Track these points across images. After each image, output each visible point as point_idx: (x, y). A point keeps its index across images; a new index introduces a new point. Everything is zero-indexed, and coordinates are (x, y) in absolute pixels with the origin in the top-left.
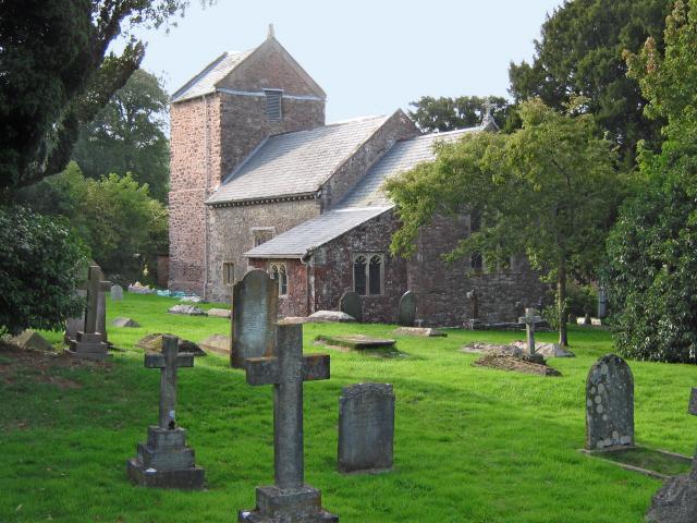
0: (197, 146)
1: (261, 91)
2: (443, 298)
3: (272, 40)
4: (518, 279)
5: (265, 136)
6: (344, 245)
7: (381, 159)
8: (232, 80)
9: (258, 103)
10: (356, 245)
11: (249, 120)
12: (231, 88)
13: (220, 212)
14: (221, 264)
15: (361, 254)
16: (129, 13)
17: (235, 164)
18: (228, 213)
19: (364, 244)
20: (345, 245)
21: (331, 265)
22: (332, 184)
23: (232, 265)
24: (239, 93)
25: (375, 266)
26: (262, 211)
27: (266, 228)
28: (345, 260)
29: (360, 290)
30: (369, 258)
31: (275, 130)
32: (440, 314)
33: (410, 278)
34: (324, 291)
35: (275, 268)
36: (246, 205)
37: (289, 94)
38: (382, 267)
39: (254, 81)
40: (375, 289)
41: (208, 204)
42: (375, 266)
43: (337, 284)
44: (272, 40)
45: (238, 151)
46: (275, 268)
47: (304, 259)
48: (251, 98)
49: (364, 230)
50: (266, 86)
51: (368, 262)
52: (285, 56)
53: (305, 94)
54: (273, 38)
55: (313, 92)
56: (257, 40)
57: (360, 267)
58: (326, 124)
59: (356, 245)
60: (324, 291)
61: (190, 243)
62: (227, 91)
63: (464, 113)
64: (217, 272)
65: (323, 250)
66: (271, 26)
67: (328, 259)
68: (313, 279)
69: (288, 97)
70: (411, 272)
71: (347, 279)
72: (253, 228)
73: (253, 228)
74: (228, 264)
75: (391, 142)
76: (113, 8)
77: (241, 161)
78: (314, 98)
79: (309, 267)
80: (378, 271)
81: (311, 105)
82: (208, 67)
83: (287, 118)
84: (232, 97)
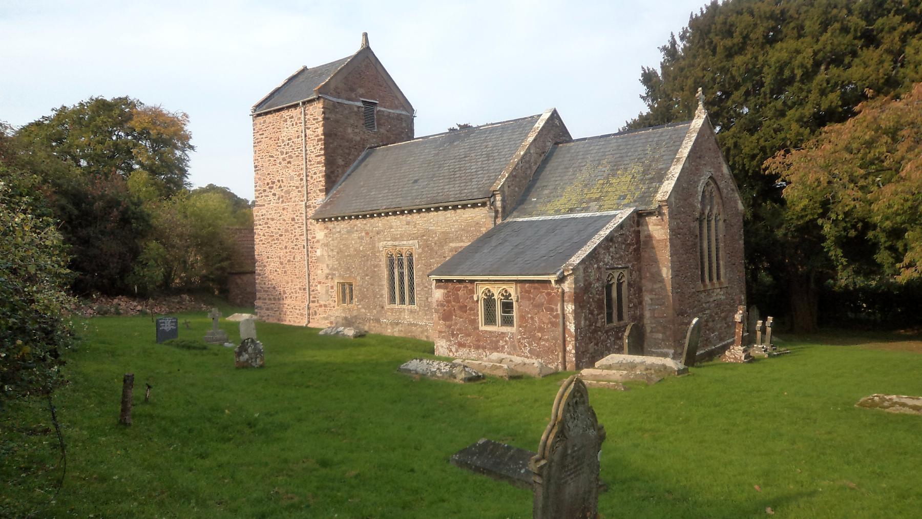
0: (290, 157)
6: (598, 262)
8: (332, 86)
9: (357, 113)
11: (350, 130)
12: (331, 95)
18: (343, 226)
22: (506, 189)
24: (340, 101)
26: (396, 222)
29: (610, 320)
37: (381, 106)
39: (352, 90)
48: (350, 107)
50: (362, 96)
51: (615, 281)
52: (378, 67)
53: (397, 108)
56: (352, 48)
61: (285, 261)
62: (328, 97)
66: (366, 35)
69: (382, 109)
75: (549, 145)
78: (404, 113)
79: (563, 292)
83: (382, 130)
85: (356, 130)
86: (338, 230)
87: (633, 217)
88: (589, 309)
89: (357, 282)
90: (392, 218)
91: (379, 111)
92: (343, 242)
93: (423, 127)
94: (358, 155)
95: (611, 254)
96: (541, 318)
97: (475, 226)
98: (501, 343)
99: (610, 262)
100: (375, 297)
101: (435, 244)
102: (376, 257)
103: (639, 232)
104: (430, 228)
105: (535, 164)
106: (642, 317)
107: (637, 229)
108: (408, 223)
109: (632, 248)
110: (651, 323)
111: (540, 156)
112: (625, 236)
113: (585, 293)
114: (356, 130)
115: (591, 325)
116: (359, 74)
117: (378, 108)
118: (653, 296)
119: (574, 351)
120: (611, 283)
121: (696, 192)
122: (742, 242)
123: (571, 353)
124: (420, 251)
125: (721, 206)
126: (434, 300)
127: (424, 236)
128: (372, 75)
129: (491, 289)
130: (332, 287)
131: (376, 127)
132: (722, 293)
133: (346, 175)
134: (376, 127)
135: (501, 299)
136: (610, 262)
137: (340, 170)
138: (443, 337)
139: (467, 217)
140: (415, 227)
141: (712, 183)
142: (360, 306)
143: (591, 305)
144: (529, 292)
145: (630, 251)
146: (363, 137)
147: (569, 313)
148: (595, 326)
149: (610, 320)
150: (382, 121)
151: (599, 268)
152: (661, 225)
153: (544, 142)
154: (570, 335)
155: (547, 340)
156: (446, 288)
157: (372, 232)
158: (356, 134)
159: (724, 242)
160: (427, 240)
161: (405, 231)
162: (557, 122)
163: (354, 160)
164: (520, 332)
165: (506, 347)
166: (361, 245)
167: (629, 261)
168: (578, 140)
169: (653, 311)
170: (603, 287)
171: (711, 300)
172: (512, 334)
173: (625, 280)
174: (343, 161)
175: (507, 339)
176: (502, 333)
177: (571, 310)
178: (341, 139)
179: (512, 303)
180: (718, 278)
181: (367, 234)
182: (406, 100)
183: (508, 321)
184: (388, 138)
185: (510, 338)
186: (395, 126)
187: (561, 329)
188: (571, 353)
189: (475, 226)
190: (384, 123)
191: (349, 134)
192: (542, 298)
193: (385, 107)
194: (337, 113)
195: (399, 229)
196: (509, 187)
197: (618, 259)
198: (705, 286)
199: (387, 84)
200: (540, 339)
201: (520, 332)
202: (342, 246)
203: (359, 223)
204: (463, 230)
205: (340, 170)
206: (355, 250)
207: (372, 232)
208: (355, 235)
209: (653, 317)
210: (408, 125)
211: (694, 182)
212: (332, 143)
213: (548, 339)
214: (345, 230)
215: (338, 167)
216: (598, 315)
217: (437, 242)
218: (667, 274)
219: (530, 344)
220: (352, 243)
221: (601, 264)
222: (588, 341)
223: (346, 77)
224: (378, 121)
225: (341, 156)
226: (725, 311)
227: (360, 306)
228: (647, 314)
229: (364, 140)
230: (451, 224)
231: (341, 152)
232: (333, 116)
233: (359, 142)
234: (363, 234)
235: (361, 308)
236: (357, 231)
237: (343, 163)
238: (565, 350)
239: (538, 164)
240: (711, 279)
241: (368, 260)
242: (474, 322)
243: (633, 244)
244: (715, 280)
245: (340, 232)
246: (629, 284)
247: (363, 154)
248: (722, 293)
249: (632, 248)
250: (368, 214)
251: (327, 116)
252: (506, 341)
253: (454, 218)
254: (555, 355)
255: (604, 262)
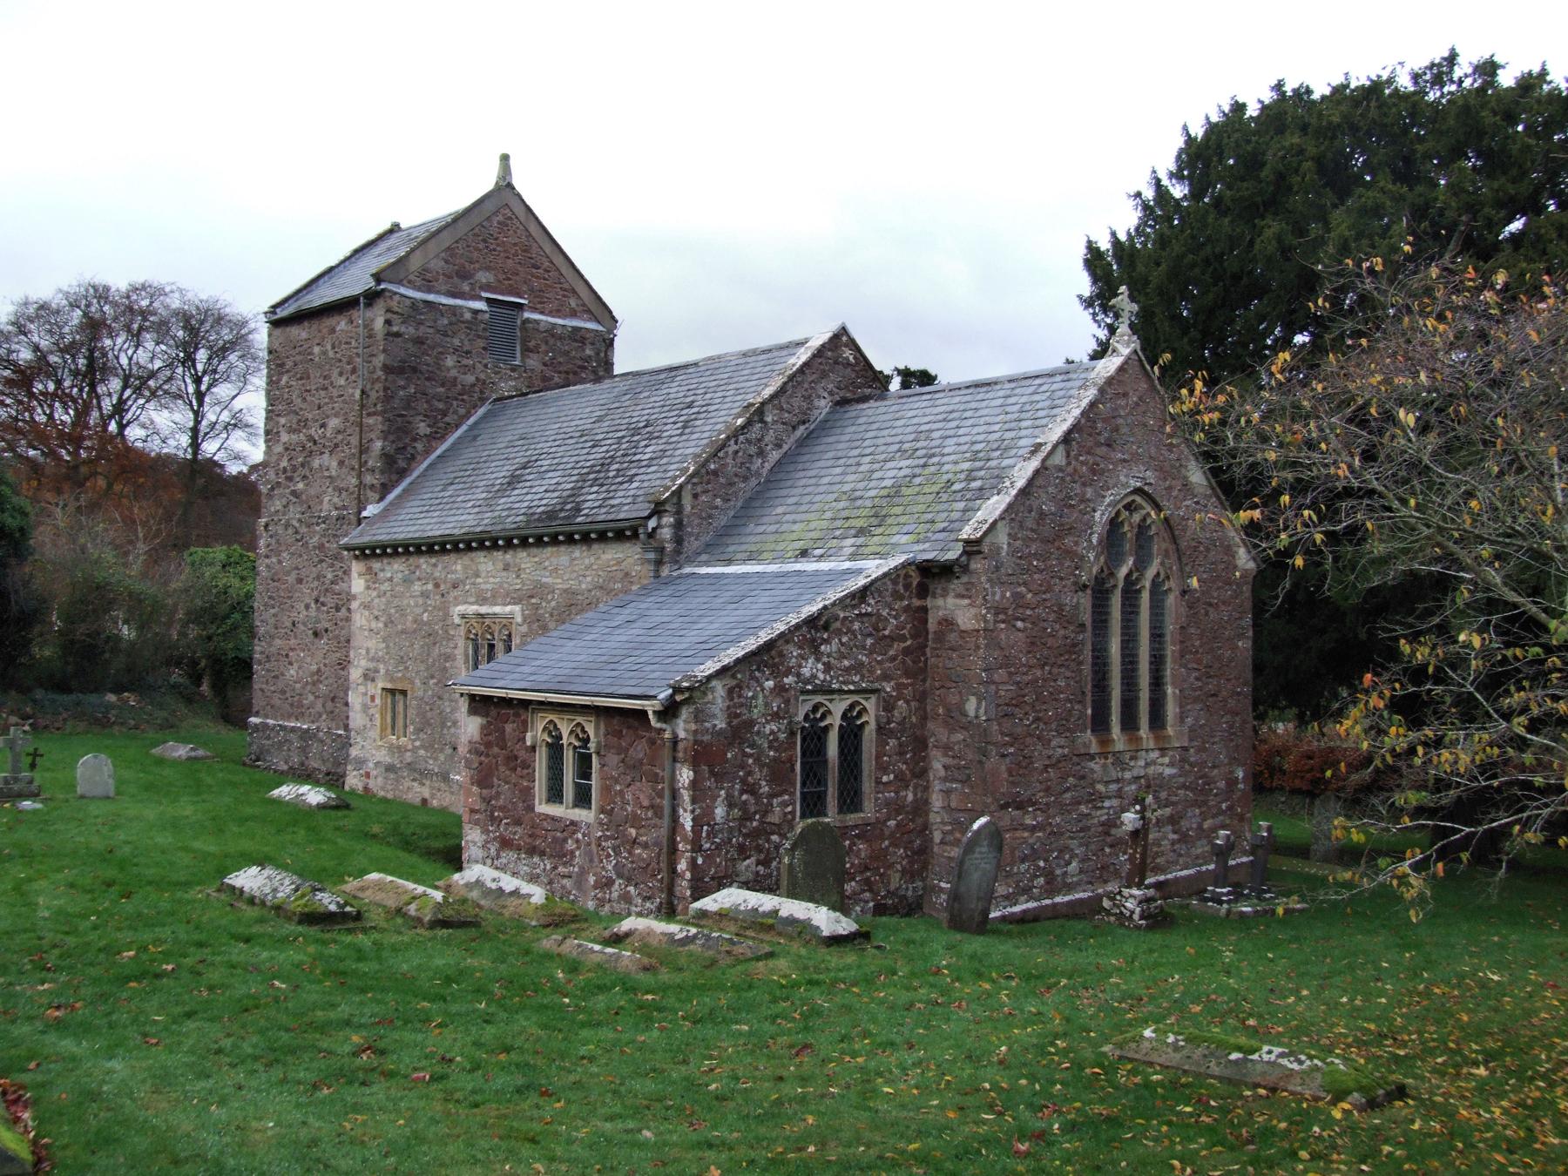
1: (480, 298)
2: (1029, 821)
3: (505, 186)
4: (1183, 760)
5: (483, 400)
7: (803, 443)
8: (416, 263)
9: (470, 325)
10: (806, 672)
11: (450, 361)
12: (411, 284)
13: (376, 565)
14: (376, 688)
15: (819, 699)
16: (229, 544)
17: (413, 457)
18: (395, 569)
19: (828, 668)
20: (777, 671)
21: (740, 730)
23: (404, 693)
24: (431, 297)
25: (851, 734)
26: (488, 566)
27: (497, 609)
28: (776, 716)
29: (814, 804)
30: (838, 707)
31: (506, 387)
32: (1023, 867)
33: (938, 764)
34: (720, 812)
35: (552, 729)
36: (444, 551)
37: (534, 310)
38: (870, 732)
39: (464, 275)
40: (851, 799)
41: (349, 548)
42: (851, 734)
43: (752, 790)
44: (505, 186)
45: (423, 428)
46: (552, 729)
47: (659, 714)
48: (453, 310)
49: (826, 627)
50: (488, 288)
51: (835, 720)
53: (573, 314)
54: (510, 186)
55: (589, 311)
56: (485, 183)
57: (814, 737)
58: (617, 370)
59: (806, 672)
60: (720, 812)
62: (402, 290)
63: (1094, 315)
64: (365, 708)
65: (719, 688)
66: (505, 158)
67: (731, 715)
68: (685, 775)
70: (947, 748)
71: (780, 775)
72: (461, 608)
73: (461, 608)
74: (392, 692)
76: (200, 367)
77: (428, 452)
79: (675, 741)
80: (857, 748)
81: (583, 341)
82: (356, 252)
84: (414, 304)
85: (465, 362)
86: (389, 575)
87: (907, 576)
88: (744, 781)
89: (418, 690)
90: (480, 557)
91: (528, 321)
92: (396, 602)
93: (625, 359)
94: (468, 416)
95: (825, 659)
96: (637, 795)
97: (622, 580)
98: (570, 845)
99: (821, 676)
100: (443, 725)
101: (552, 615)
102: (450, 638)
103: (925, 610)
104: (544, 580)
105: (779, 446)
106: (921, 807)
107: (916, 602)
108: (506, 568)
109: (897, 647)
110: (943, 823)
111: (794, 428)
112: (874, 619)
113: (731, 744)
114: (465, 362)
115: (746, 817)
116: (485, 241)
117: (527, 315)
118: (949, 761)
119: (688, 875)
120: (822, 724)
121: (1090, 525)
122: (1245, 645)
123: (683, 879)
124: (524, 629)
125: (1174, 557)
126: (464, 739)
127: (532, 597)
128: (515, 244)
129: (556, 721)
130: (373, 698)
131: (518, 355)
132: (1167, 760)
133: (433, 456)
134: (518, 355)
135: (575, 747)
136: (821, 676)
137: (419, 446)
138: (477, 823)
139: (609, 560)
140: (518, 576)
141: (1144, 504)
142: (418, 743)
143: (750, 773)
144: (619, 734)
145: (891, 653)
146: (482, 376)
147: (684, 788)
148: (762, 822)
149: (814, 804)
150: (532, 344)
151: (780, 689)
152: (970, 597)
153: (808, 398)
154: (685, 839)
155: (645, 846)
156: (487, 715)
157: (445, 582)
158: (467, 369)
159: (1182, 642)
160: (537, 607)
161: (501, 585)
162: (848, 354)
163: (457, 426)
164: (601, 824)
165: (577, 853)
166: (426, 611)
167: (886, 677)
168: (954, 389)
169: (947, 793)
170: (792, 734)
171: (1128, 775)
172: (588, 825)
173: (870, 719)
174: (429, 426)
175: (580, 836)
176: (573, 823)
177: (687, 781)
178: (428, 379)
179: (590, 756)
180: (1157, 720)
181: (437, 586)
182: (599, 298)
183: (583, 799)
184: (545, 379)
185: (584, 835)
186: (567, 353)
187: (666, 821)
188: (683, 879)
189: (622, 580)
190: (538, 346)
191: (448, 370)
192: (640, 750)
193: (542, 313)
194: (421, 323)
195: (492, 580)
196: (695, 496)
197: (847, 670)
198: (1105, 741)
199: (552, 262)
200: (634, 842)
201: (601, 824)
202: (393, 611)
203: (424, 563)
204: (601, 588)
205: (419, 446)
206: (415, 621)
207: (445, 582)
208: (417, 587)
209: (947, 808)
210: (598, 354)
211: (1082, 501)
212: (404, 388)
213: (646, 843)
214: (400, 575)
215: (415, 440)
216: (772, 796)
217: (555, 612)
218: (977, 709)
219: (618, 854)
220: (409, 605)
221: (789, 680)
222: (733, 853)
223: (449, 248)
224: (524, 341)
225: (425, 416)
226: (1173, 804)
227: (418, 743)
228: (937, 801)
229: (484, 382)
230: (581, 573)
231: (425, 406)
232: (412, 330)
233: (473, 385)
234: (430, 586)
235: (418, 748)
236: (419, 579)
237: (428, 431)
238: (673, 870)
239: (786, 447)
240: (1129, 723)
241: (435, 644)
242: (527, 794)
243: (903, 638)
244: (1144, 731)
245: (391, 579)
246: (880, 729)
247: (481, 411)
248: (1167, 760)
249: (897, 647)
250: (547, 535)
251: (395, 329)
252: (577, 841)
253: (587, 561)
254: (658, 881)
255: (798, 675)
